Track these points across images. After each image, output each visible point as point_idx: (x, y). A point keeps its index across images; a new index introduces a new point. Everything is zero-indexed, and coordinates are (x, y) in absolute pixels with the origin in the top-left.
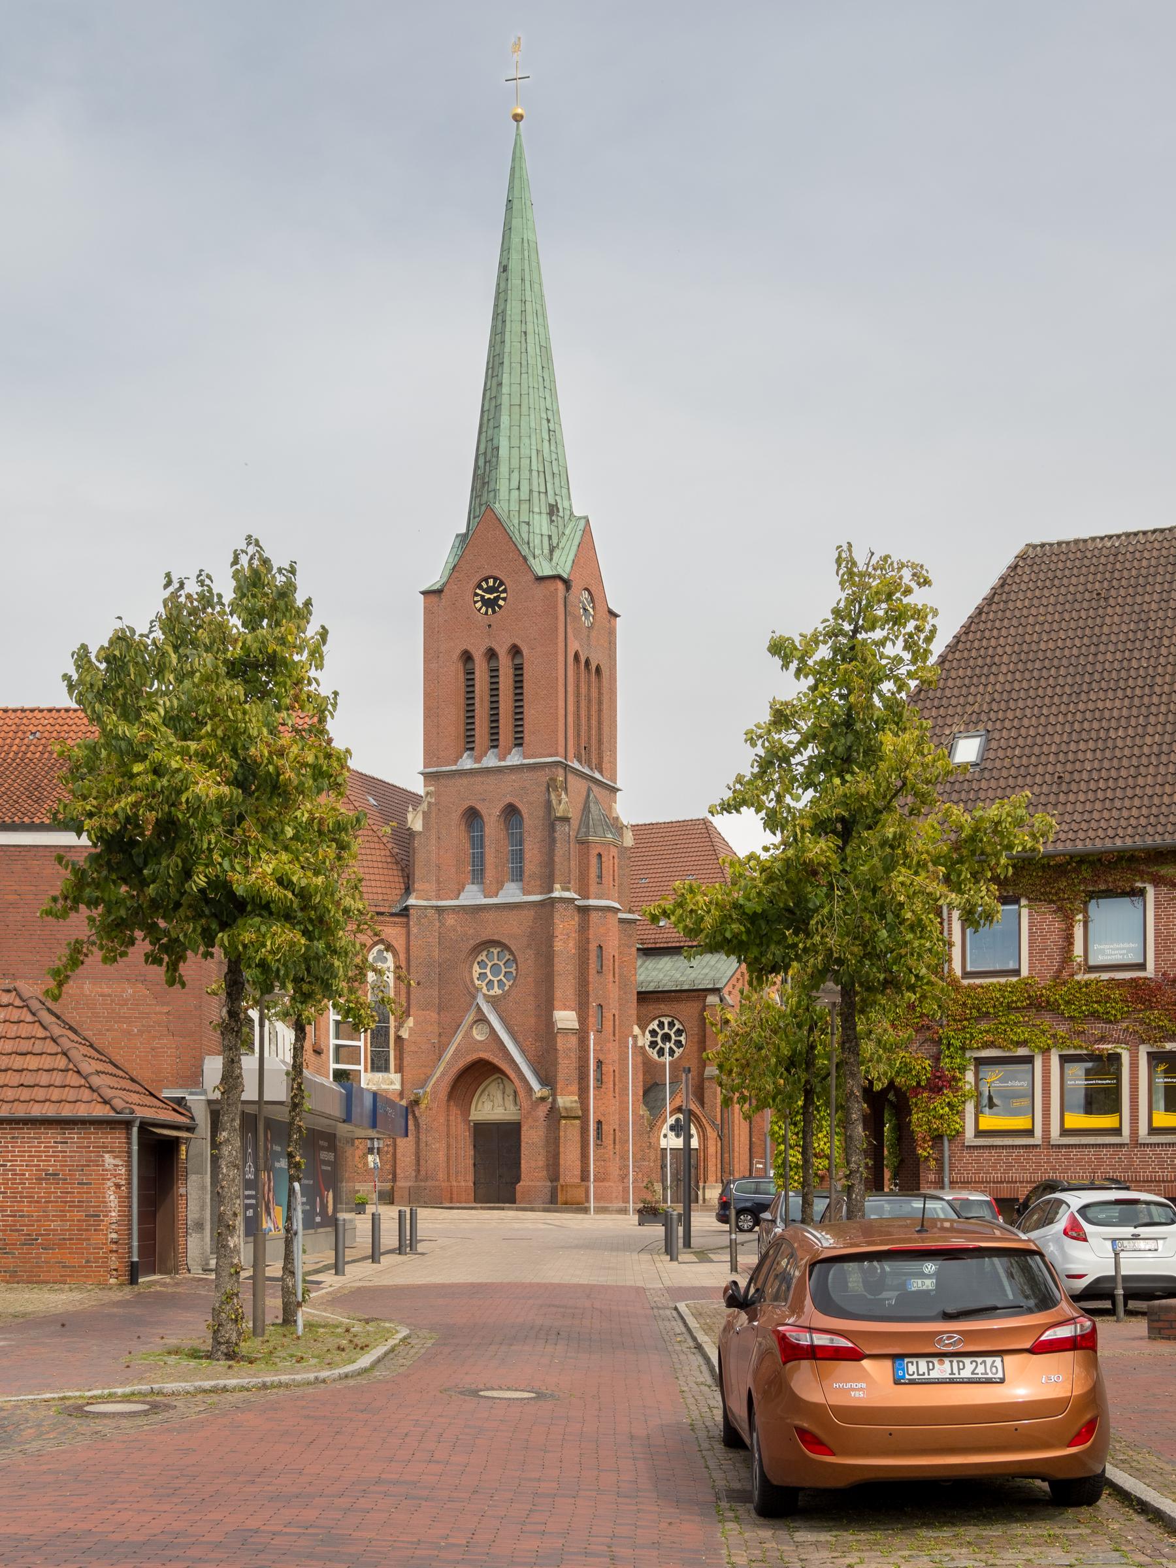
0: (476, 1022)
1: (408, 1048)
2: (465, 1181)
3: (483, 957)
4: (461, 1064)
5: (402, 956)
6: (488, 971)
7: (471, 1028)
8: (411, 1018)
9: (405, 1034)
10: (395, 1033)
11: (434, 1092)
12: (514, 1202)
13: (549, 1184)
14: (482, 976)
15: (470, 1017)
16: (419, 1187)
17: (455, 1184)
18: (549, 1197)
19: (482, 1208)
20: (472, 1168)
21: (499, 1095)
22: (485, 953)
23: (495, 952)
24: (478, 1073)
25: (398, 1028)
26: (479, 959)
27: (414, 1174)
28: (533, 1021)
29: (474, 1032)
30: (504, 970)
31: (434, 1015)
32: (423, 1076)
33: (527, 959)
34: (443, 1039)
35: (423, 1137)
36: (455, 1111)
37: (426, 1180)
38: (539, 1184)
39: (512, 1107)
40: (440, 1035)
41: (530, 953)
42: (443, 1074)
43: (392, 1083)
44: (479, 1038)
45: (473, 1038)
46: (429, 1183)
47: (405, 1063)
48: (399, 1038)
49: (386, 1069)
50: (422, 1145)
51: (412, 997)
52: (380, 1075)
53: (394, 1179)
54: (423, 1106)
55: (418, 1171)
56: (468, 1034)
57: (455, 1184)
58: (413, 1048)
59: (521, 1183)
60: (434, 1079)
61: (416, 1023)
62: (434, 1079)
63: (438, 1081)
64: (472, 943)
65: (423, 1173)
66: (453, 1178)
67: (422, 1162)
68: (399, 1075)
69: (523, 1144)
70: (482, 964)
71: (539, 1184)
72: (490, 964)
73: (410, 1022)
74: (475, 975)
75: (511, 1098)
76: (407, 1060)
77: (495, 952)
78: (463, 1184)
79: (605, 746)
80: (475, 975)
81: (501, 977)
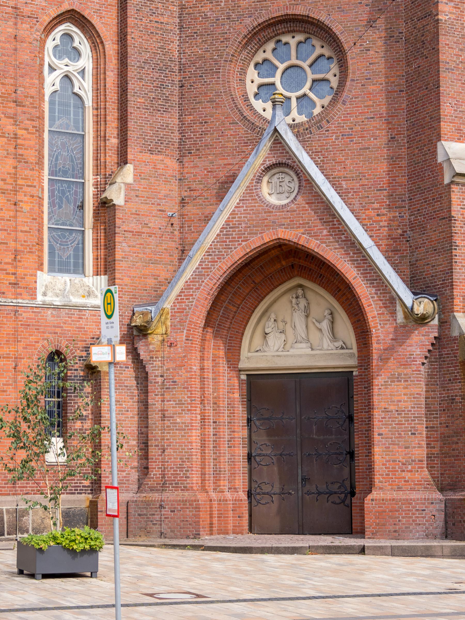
0: (268, 169)
1: (123, 224)
2: (234, 490)
3: (267, 52)
4: (237, 253)
5: (111, 48)
6: (277, 79)
7: (259, 180)
8: (129, 168)
9: (117, 195)
10: (96, 196)
11: (179, 311)
12: (361, 533)
13: (438, 495)
14: (266, 89)
15: (262, 155)
16: (148, 503)
17: (213, 495)
18: (440, 522)
19: (314, 550)
20: (242, 466)
21: (299, 319)
22: (271, 45)
23: (293, 42)
24: (274, 268)
25: (101, 187)
26: (259, 57)
27: (134, 476)
28: (382, 168)
29: (265, 189)
30: (310, 76)
31: (172, 164)
32: (151, 282)
33: (370, 54)
34: (190, 209)
35: (155, 401)
36: (216, 349)
37: (163, 487)
38: (414, 495)
39: (327, 343)
40: (183, 202)
41: (376, 39)
42: (199, 274)
43: (89, 294)
44: (274, 200)
45: (263, 201)
46: (170, 496)
47: (119, 255)
48: (105, 206)
49: (78, 268)
50: (154, 416)
51: (131, 124)
52: (66, 277)
53: (97, 486)
54: (155, 339)
55: (145, 470)
56: (252, 192)
57: (213, 495)
58: (133, 226)
59: (374, 494)
60: (181, 284)
61: (138, 176)
62: (181, 284)
63: (188, 286)
64: (250, 23)
65: (155, 472)
66: (210, 485)
67: (153, 452)
68: (104, 279)
69: (377, 415)
70: (265, 66)
71: (414, 495)
72: (282, 67)
73: (128, 174)
74: (251, 89)
75: (325, 325)
76: (122, 247)
77: (293, 42)
78: (228, 495)
79: (95, 77)
80: (251, 89)
81: (293, 95)
